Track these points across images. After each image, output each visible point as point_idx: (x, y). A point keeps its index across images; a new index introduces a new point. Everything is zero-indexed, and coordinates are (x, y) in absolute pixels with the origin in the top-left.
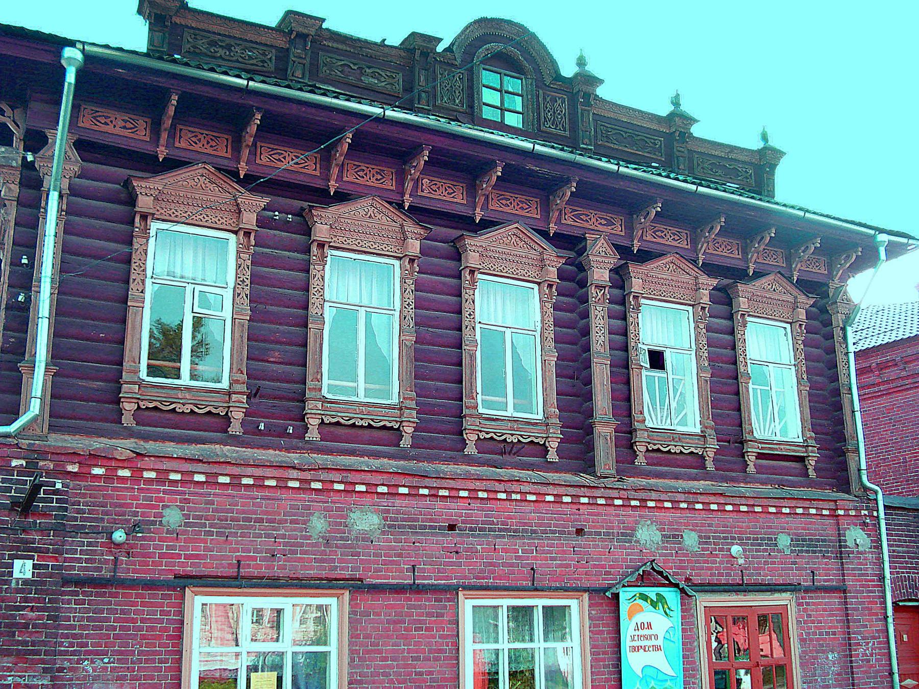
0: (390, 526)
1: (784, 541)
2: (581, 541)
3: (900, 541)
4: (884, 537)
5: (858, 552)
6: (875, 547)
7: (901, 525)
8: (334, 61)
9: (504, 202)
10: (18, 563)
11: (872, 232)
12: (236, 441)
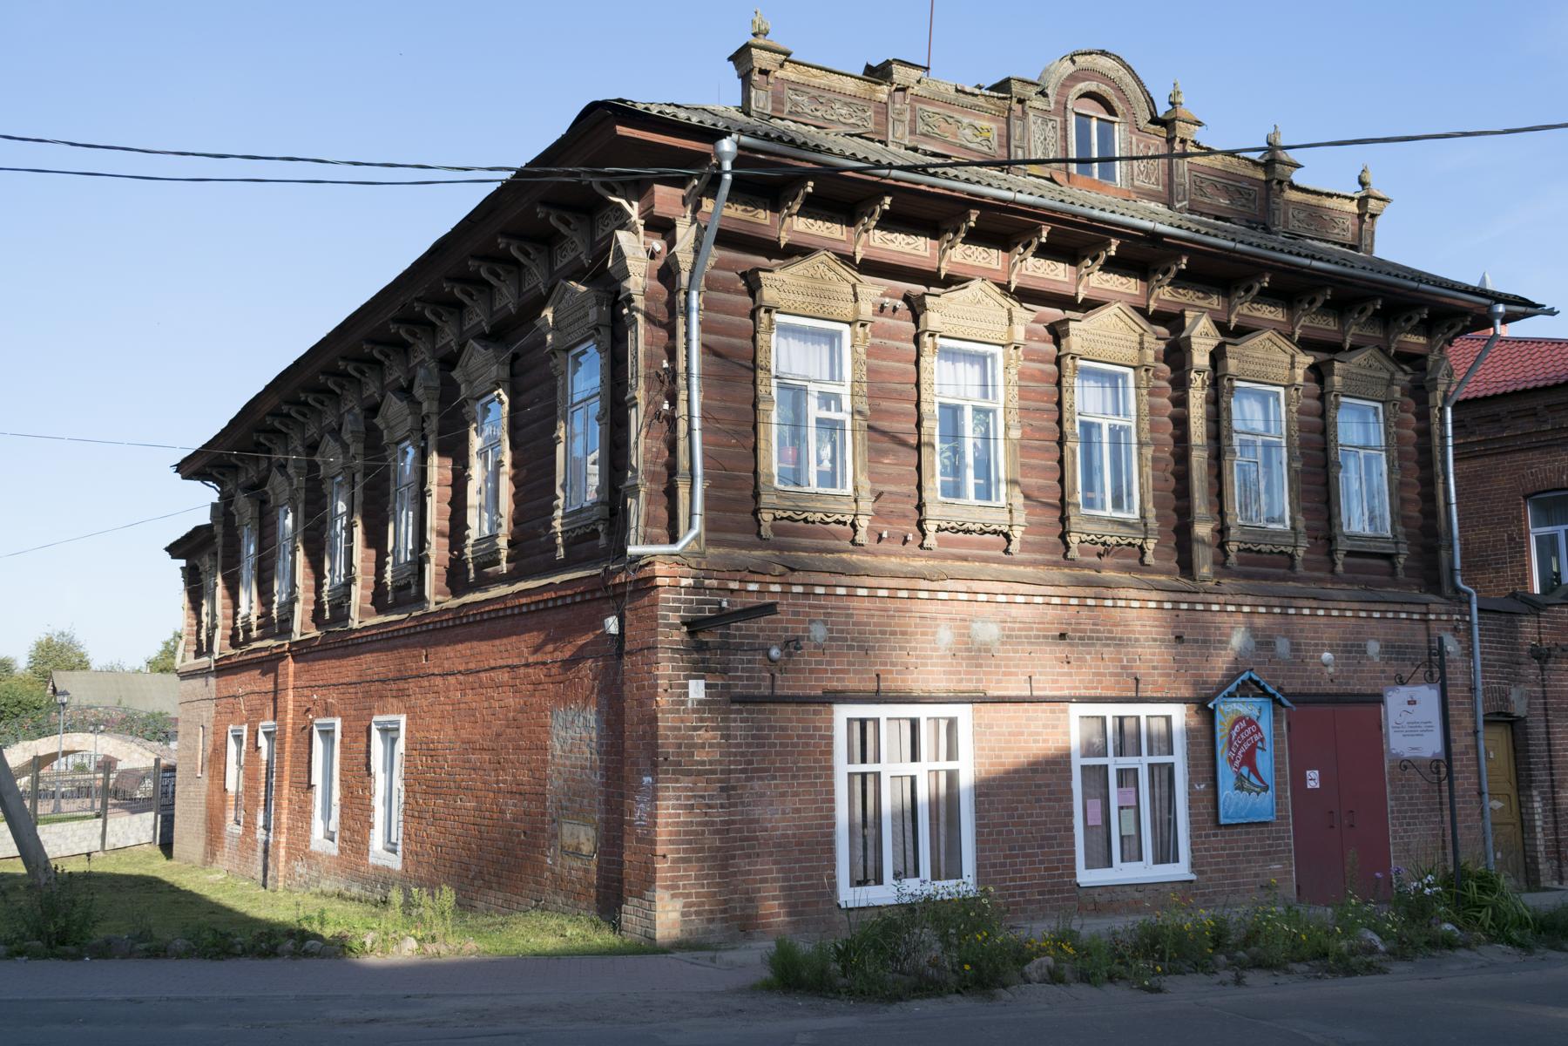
0: (1008, 636)
1: (1373, 648)
3: (1490, 648)
4: (1477, 645)
6: (1466, 655)
7: (1492, 630)
11: (1487, 302)
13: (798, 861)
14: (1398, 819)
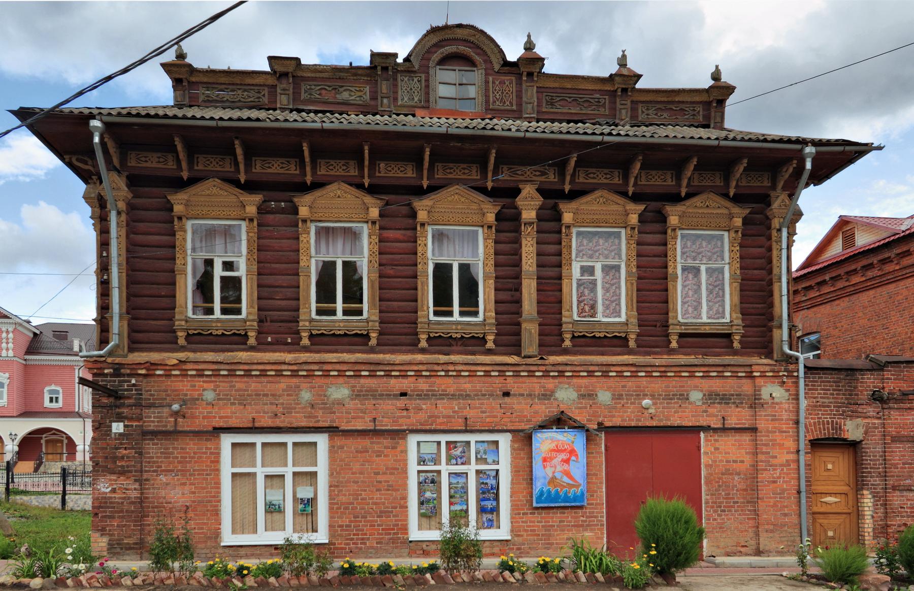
2: (507, 399)
5: (773, 403)
8: (313, 87)
9: (448, 171)
10: (114, 425)
11: (798, 147)
12: (252, 349)
13: (204, 524)
14: (712, 507)
